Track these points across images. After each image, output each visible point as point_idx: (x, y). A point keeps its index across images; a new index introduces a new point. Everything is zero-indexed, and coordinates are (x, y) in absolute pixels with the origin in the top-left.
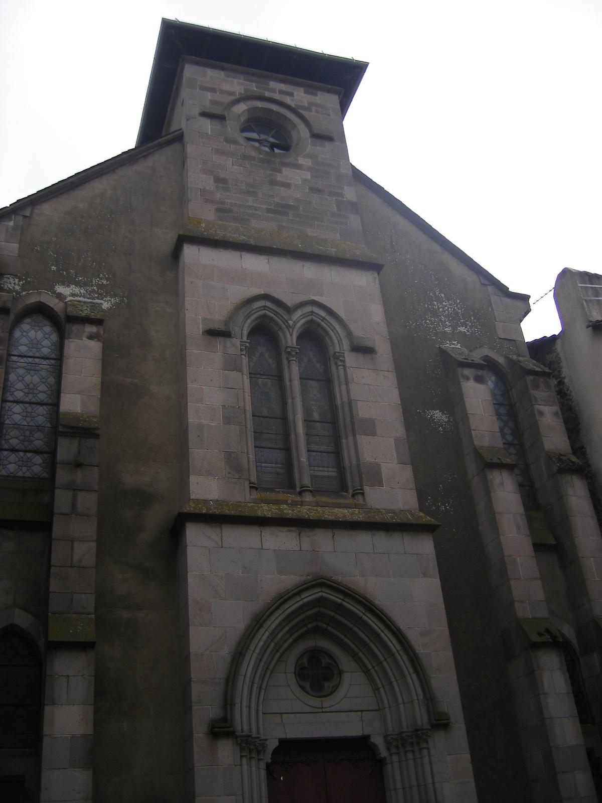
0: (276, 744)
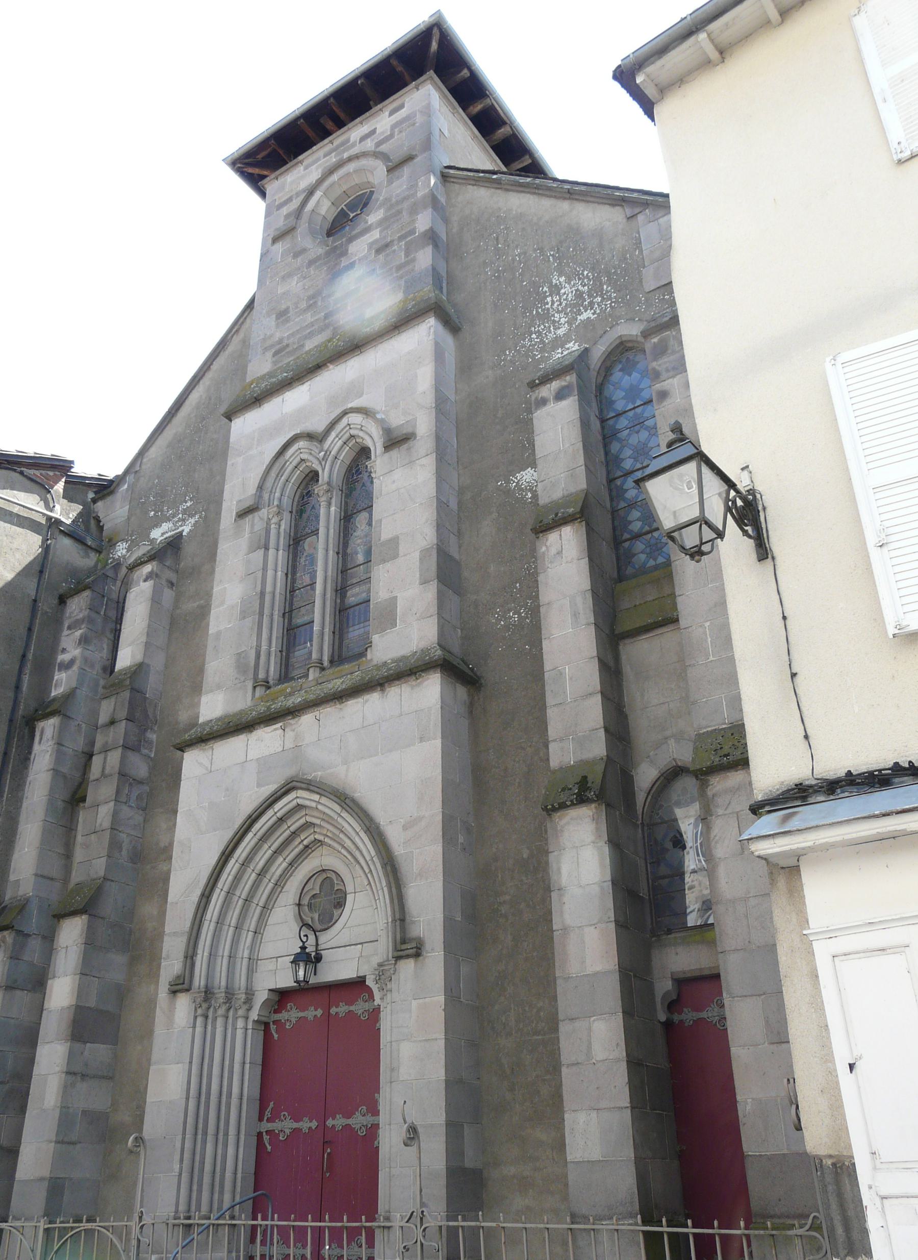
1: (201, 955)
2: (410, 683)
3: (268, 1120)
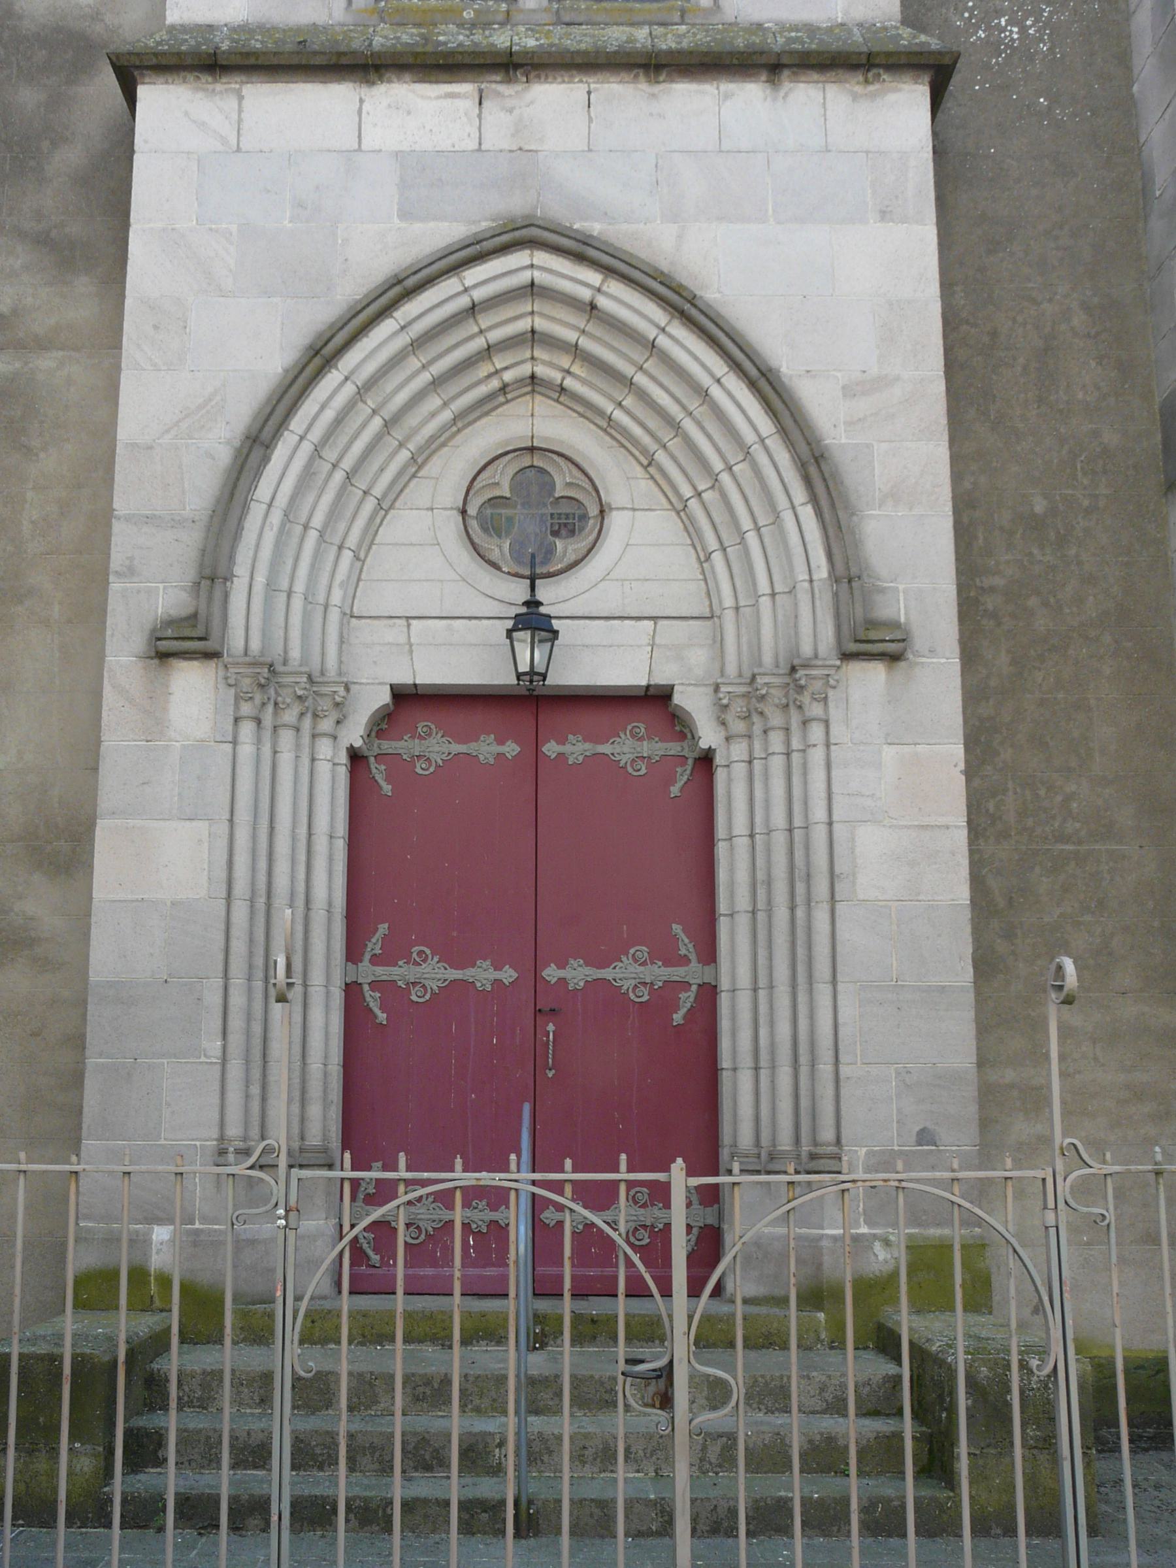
0: (384, 697)
1: (246, 580)
2: (847, 85)
3: (376, 960)
